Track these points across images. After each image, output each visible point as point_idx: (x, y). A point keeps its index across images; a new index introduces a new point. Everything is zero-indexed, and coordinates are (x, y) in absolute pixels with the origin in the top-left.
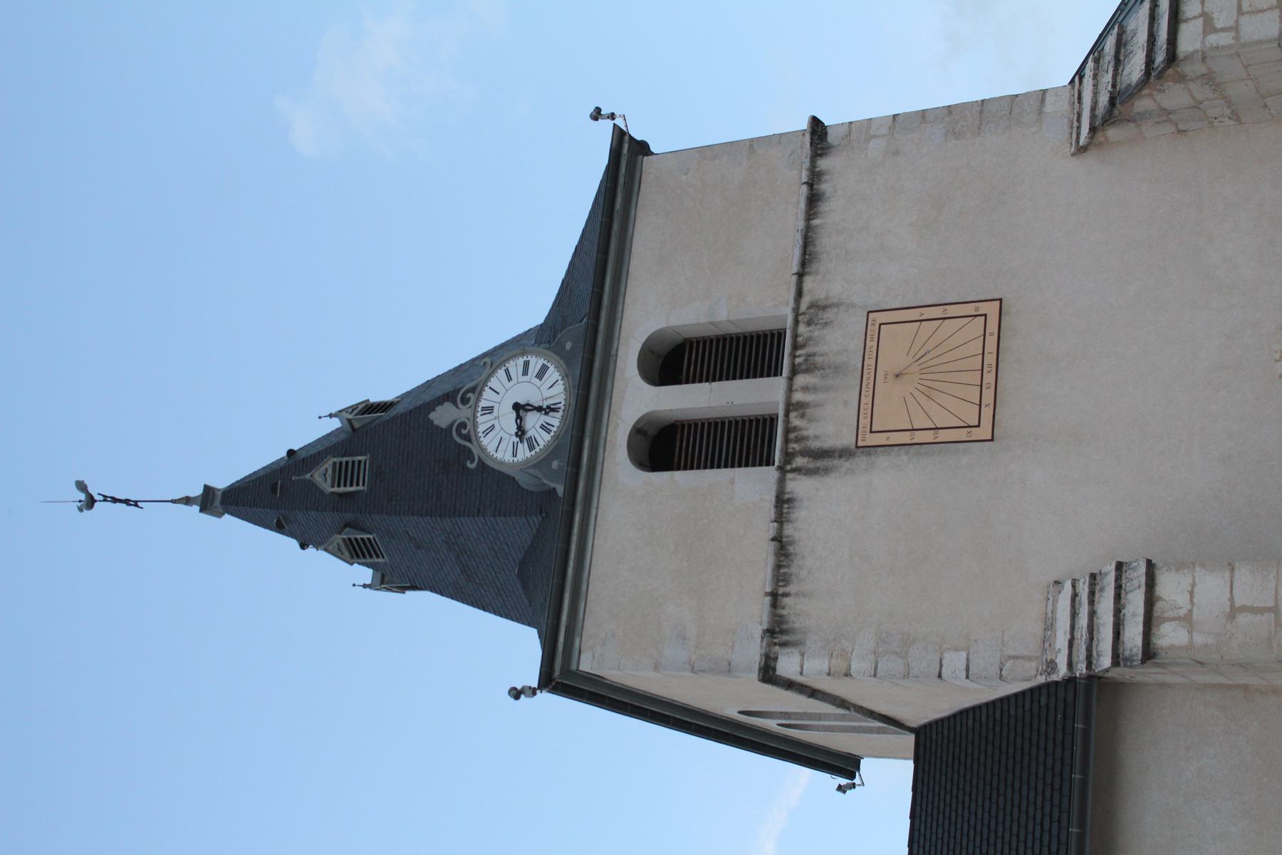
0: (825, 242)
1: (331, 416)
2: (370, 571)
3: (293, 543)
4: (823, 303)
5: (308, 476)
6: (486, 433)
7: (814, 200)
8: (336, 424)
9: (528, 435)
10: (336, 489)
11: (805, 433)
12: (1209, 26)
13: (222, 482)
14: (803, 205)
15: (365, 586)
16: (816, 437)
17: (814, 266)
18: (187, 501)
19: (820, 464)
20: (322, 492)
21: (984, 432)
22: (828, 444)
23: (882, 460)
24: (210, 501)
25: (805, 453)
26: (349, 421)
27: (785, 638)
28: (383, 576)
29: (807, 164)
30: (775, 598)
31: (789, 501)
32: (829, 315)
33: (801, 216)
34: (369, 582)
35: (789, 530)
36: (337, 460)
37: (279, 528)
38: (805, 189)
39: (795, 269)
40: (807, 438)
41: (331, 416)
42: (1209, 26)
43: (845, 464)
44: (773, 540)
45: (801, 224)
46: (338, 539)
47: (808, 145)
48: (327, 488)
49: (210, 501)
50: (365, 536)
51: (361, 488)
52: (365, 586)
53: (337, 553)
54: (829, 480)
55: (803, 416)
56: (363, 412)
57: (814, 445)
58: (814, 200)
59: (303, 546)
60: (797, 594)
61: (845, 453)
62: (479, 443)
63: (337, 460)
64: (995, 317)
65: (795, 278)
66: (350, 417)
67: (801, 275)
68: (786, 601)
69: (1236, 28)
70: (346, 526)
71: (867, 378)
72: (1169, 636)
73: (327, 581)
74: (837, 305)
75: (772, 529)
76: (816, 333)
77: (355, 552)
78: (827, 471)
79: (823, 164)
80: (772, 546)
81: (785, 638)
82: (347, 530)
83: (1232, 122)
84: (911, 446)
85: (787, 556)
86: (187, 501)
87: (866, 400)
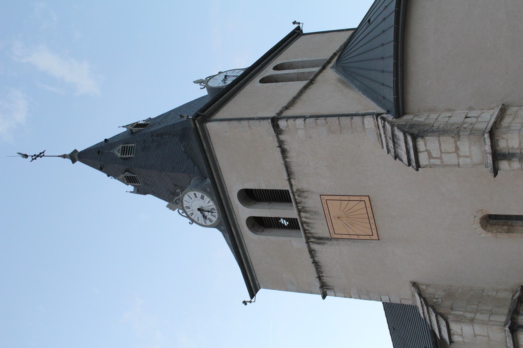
0: (294, 168)
1: (123, 127)
2: (133, 187)
3: (106, 175)
4: (302, 190)
5: (112, 151)
6: (195, 194)
7: (284, 152)
8: (125, 129)
9: (208, 217)
10: (122, 156)
11: (311, 232)
12: (430, 156)
13: (80, 149)
14: (280, 155)
15: (131, 192)
16: (316, 233)
17: (293, 176)
18: (64, 156)
19: (320, 241)
20: (116, 156)
21: (375, 237)
22: (321, 236)
23: (341, 242)
24: (75, 157)
25: (314, 238)
26: (131, 130)
27: (327, 287)
28: (138, 190)
29: (276, 139)
30: (320, 278)
31: (313, 250)
32: (305, 194)
33: (282, 159)
34: (133, 191)
35: (316, 259)
36: (124, 145)
37: (101, 169)
38: (279, 149)
39: (287, 178)
40: (313, 233)
41: (123, 127)
42: (430, 156)
43: (330, 242)
44: (313, 263)
45: (283, 162)
46: (122, 176)
47: (273, 132)
48: (119, 155)
49: (75, 157)
50: (133, 175)
51: (132, 156)
52: (131, 192)
53: (123, 181)
54: (325, 246)
55: (308, 226)
56: (136, 127)
57: (316, 235)
58: (284, 152)
59: (109, 176)
60: (326, 277)
61: (327, 239)
62: (183, 196)
63: (124, 145)
64: (375, 236)
65: (287, 181)
66: (131, 128)
67: (289, 180)
68: (323, 278)
69: (441, 158)
70: (126, 171)
71: (327, 216)
72: (455, 338)
73: (116, 190)
74: (307, 191)
75: (311, 260)
76: (303, 200)
77: (129, 181)
78: (323, 244)
79: (282, 137)
80: (313, 265)
81: (327, 287)
82: (127, 173)
83: (354, 100)
84: (350, 239)
85: (319, 266)
86: (64, 156)
87: (330, 224)
